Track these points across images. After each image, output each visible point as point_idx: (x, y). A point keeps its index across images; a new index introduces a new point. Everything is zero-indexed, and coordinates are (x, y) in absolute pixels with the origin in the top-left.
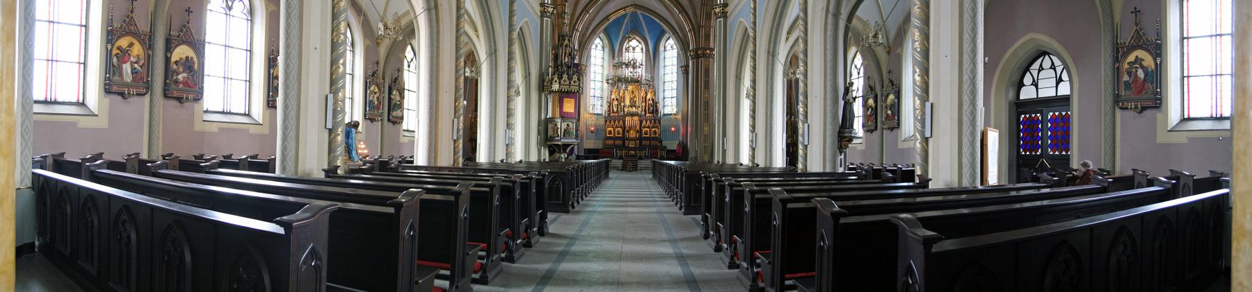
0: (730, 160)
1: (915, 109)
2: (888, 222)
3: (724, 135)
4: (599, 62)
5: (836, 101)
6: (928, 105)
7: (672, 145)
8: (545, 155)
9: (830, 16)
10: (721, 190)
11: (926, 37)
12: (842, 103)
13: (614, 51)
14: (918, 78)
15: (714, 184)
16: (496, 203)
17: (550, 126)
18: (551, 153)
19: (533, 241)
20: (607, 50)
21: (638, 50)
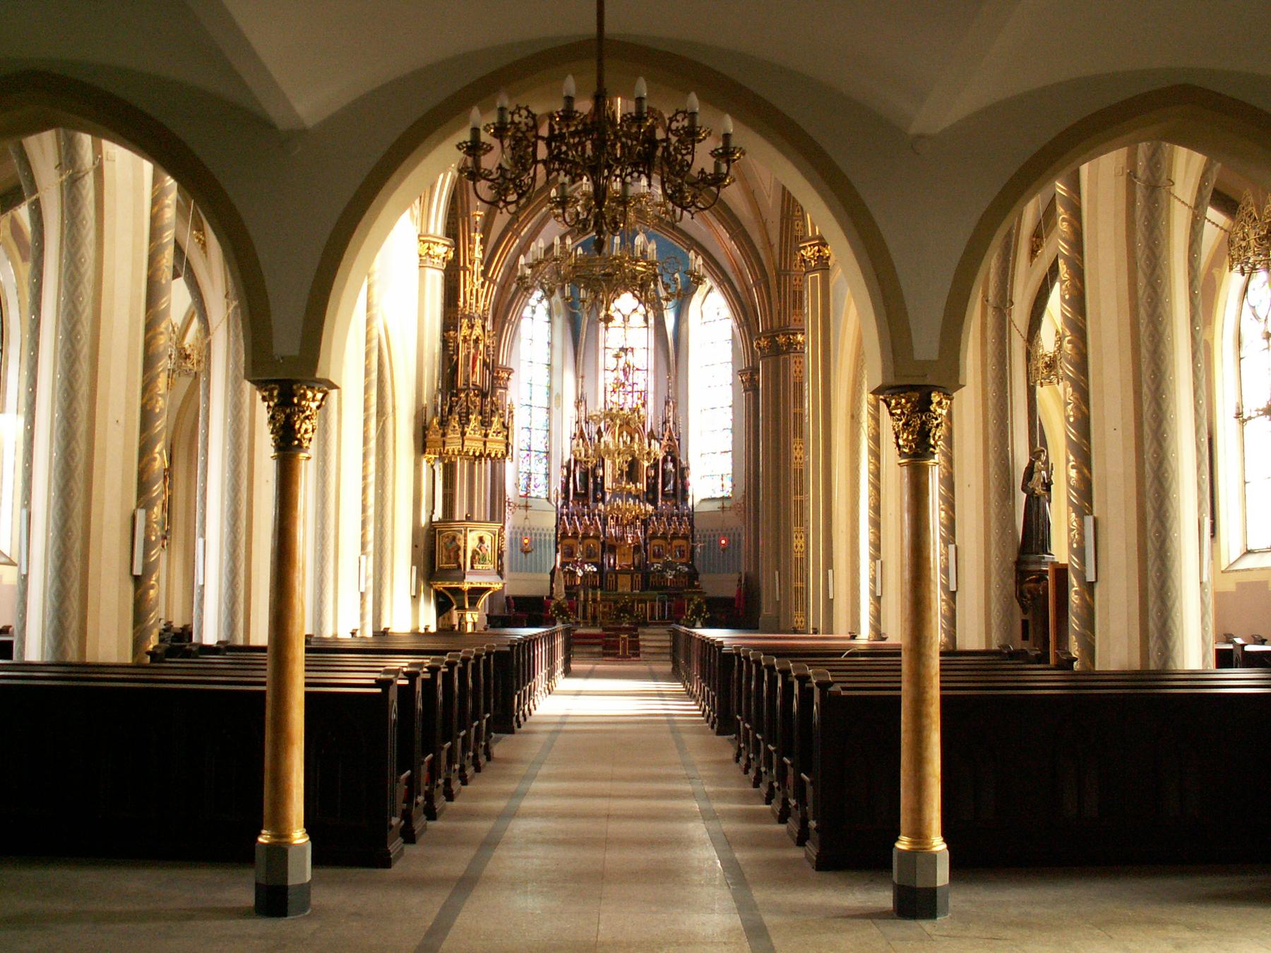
0: (1116, 650)
1: (1070, 530)
2: (955, 711)
3: (829, 563)
4: (542, 354)
5: (1006, 493)
6: (1089, 520)
7: (722, 585)
8: (428, 618)
9: (990, 311)
10: (806, 694)
11: (950, 460)
12: (1021, 498)
13: (579, 331)
14: (1073, 473)
15: (817, 692)
16: (394, 716)
17: (440, 542)
18: (443, 607)
19: (417, 826)
20: (559, 321)
21: (637, 319)
